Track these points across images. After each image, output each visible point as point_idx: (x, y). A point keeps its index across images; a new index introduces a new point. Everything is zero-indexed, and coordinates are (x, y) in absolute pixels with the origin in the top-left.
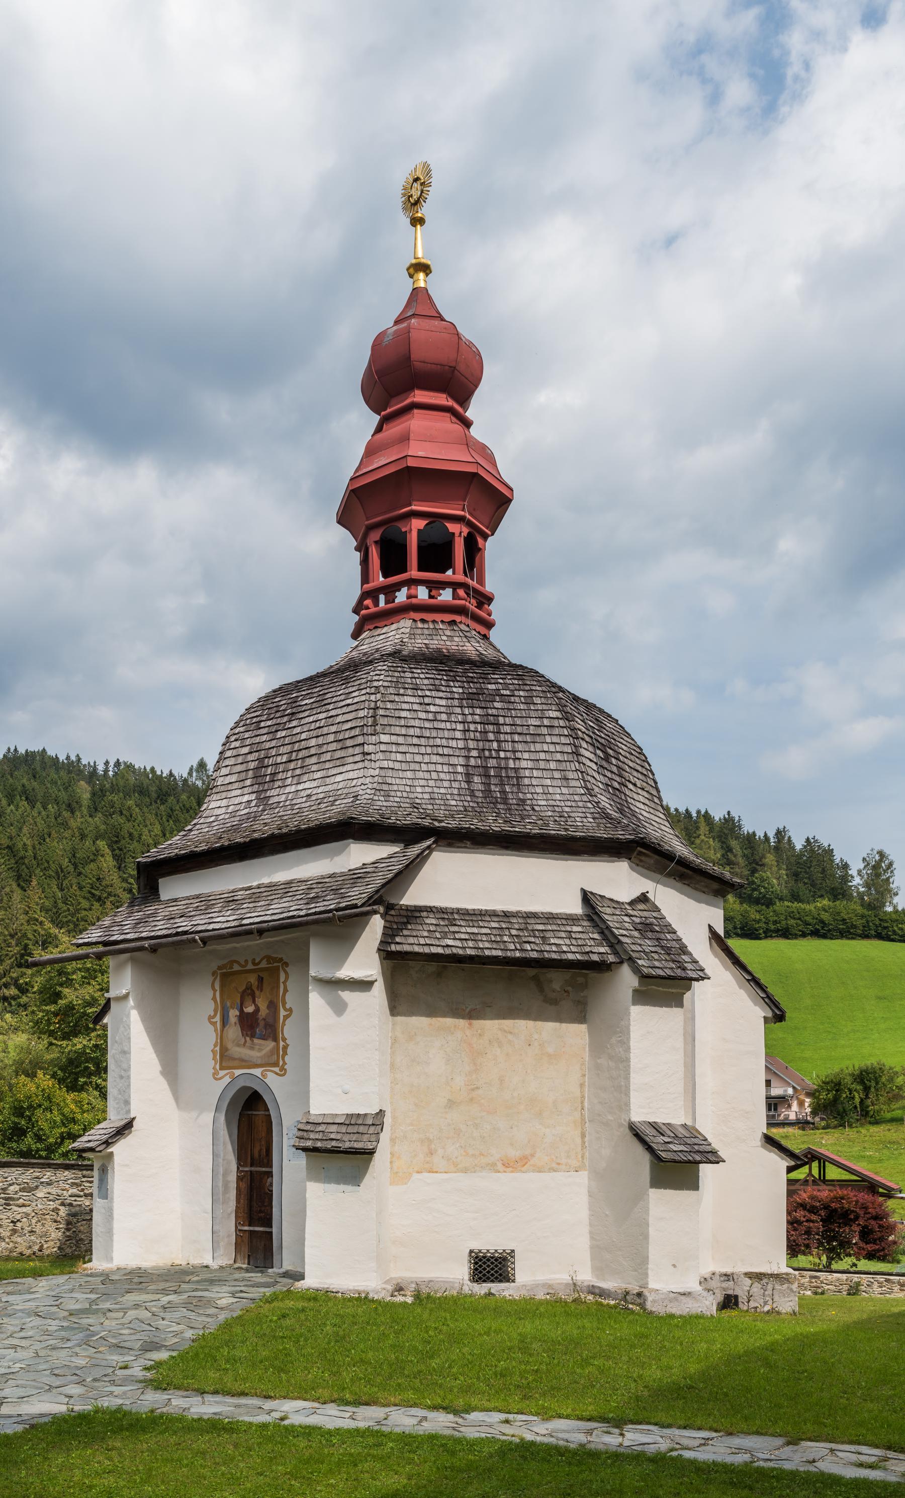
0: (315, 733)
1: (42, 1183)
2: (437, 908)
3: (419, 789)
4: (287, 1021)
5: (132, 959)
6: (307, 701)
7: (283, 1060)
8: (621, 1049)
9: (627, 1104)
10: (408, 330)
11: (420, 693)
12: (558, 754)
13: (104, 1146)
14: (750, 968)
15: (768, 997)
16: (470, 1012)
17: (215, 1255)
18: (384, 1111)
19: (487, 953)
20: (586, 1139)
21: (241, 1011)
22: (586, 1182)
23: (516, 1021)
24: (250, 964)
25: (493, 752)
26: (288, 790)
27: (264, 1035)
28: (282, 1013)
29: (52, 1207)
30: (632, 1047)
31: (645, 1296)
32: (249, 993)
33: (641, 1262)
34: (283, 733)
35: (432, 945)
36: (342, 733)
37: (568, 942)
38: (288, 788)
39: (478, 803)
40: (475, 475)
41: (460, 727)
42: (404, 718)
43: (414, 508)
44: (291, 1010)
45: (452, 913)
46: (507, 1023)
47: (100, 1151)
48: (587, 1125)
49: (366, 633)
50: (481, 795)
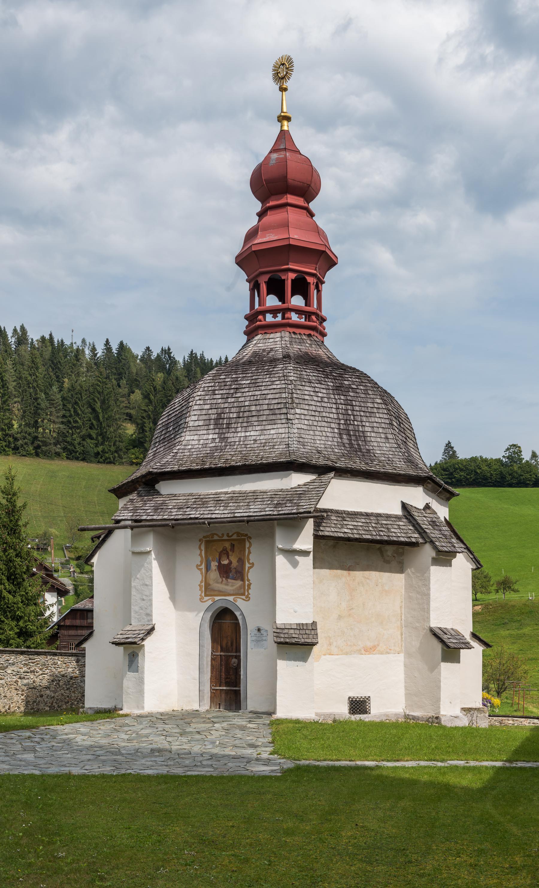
0: (254, 403)
1: (10, 664)
2: (334, 510)
3: (318, 442)
4: (251, 570)
5: (154, 531)
6: (244, 382)
7: (248, 591)
8: (424, 589)
9: (428, 618)
10: (285, 160)
11: (313, 385)
12: (383, 424)
13: (141, 641)
14: (465, 542)
15: (474, 558)
16: (349, 567)
17: (201, 704)
18: (316, 622)
19: (364, 537)
20: (403, 636)
21: (219, 563)
22: (403, 659)
23: (371, 572)
24: (225, 536)
25: (351, 421)
26: (239, 435)
27: (235, 577)
28: (247, 565)
29: (15, 680)
30: (431, 588)
31: (440, 718)
32: (225, 553)
33: (436, 701)
34: (233, 400)
35: (338, 532)
36: (272, 405)
37: (399, 531)
38: (239, 433)
39: (348, 451)
40: (324, 252)
41: (334, 406)
42: (307, 399)
43: (291, 267)
44: (253, 564)
45: (342, 513)
46: (367, 573)
47: (139, 644)
48: (403, 628)
49: (260, 336)
50: (348, 446)
